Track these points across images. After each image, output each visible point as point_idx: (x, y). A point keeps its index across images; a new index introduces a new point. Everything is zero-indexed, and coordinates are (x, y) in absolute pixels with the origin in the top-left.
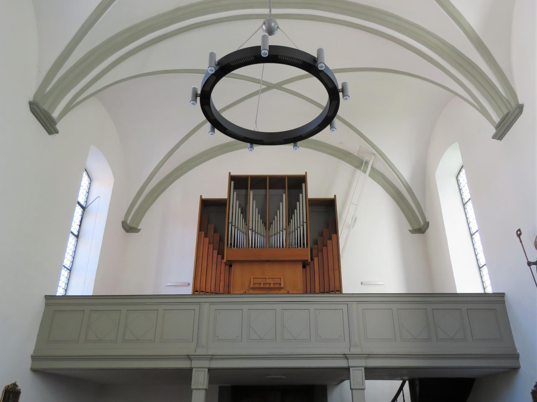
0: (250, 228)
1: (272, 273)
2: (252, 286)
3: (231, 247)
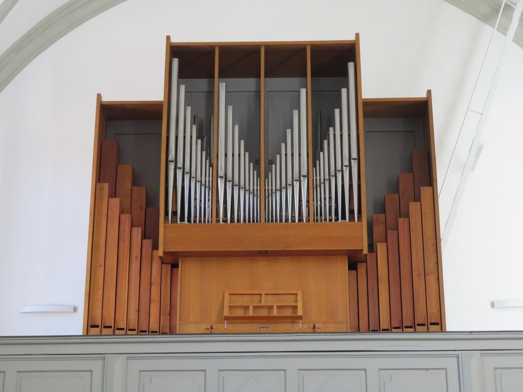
0: (221, 173)
1: (273, 281)
2: (226, 313)
3: (174, 221)
